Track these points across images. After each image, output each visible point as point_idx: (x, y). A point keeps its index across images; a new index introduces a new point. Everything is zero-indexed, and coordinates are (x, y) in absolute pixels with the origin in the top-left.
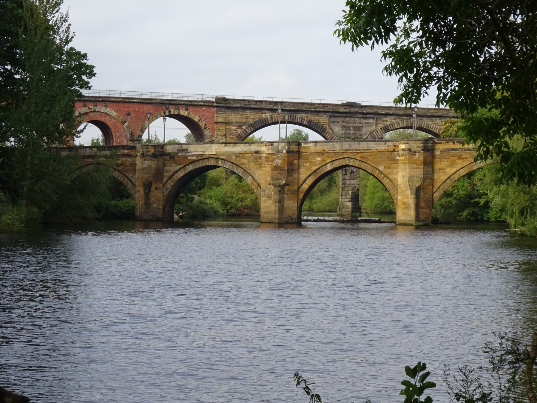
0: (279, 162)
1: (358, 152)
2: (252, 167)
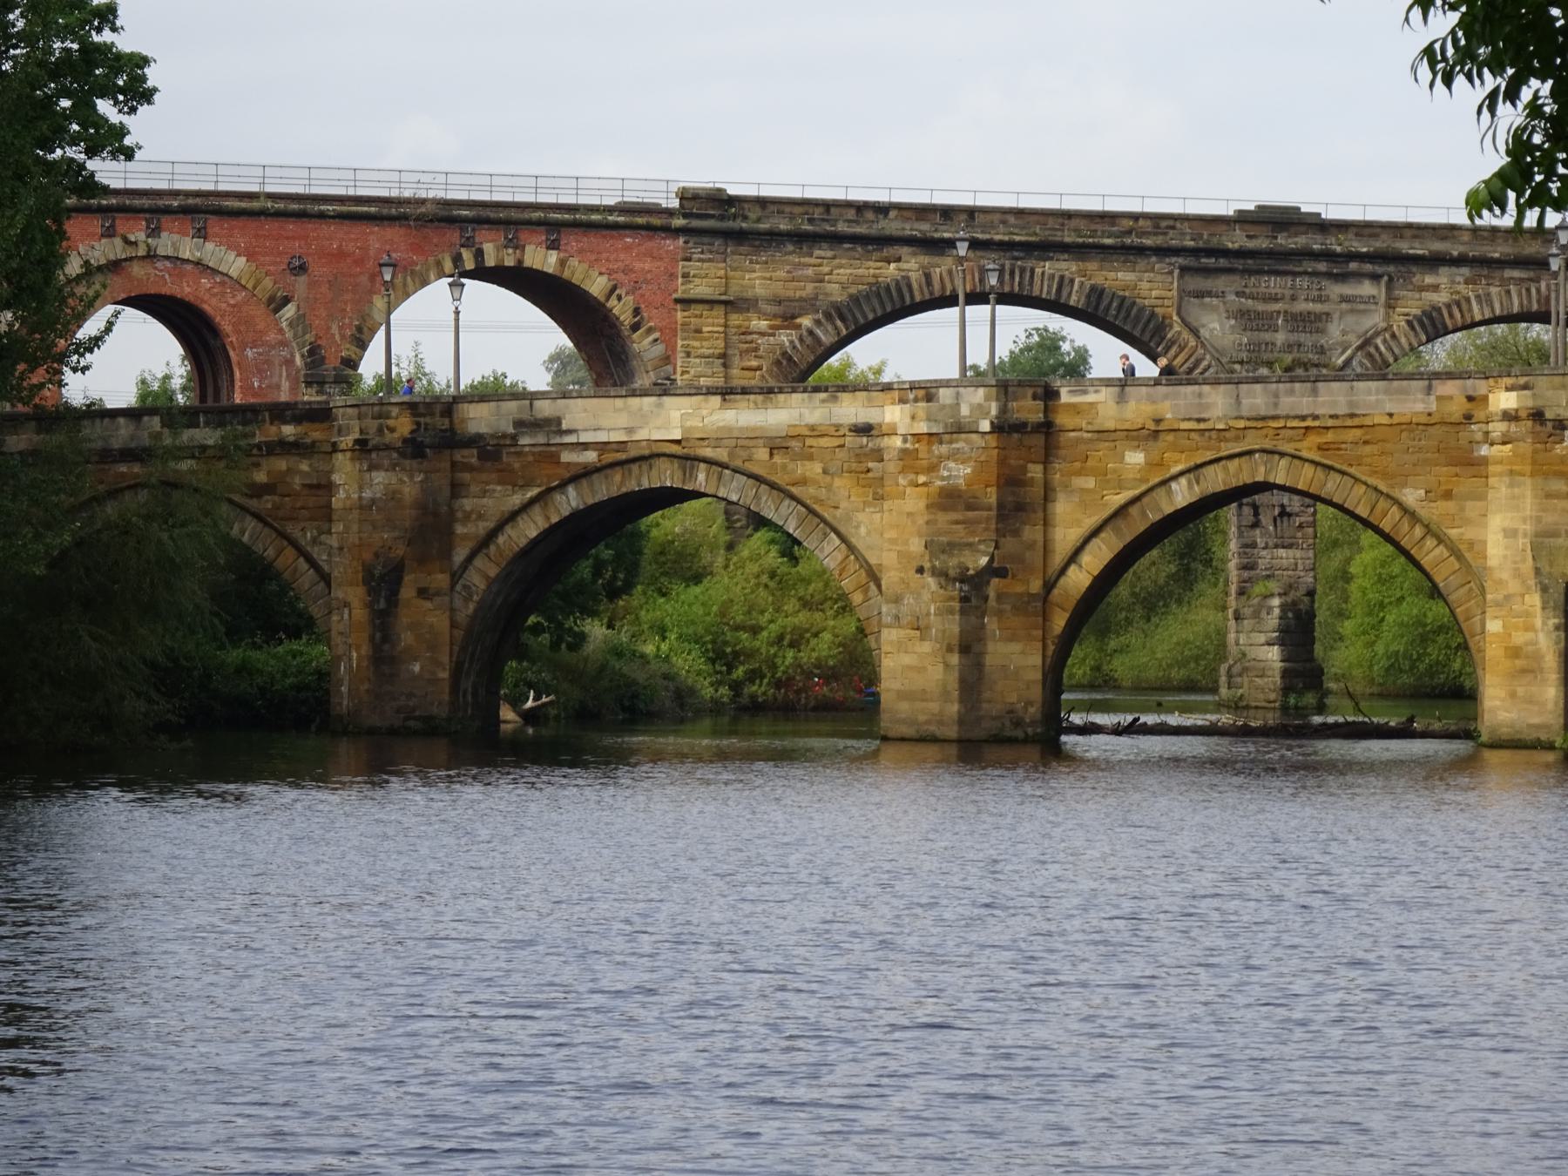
0: (959, 473)
1: (1309, 425)
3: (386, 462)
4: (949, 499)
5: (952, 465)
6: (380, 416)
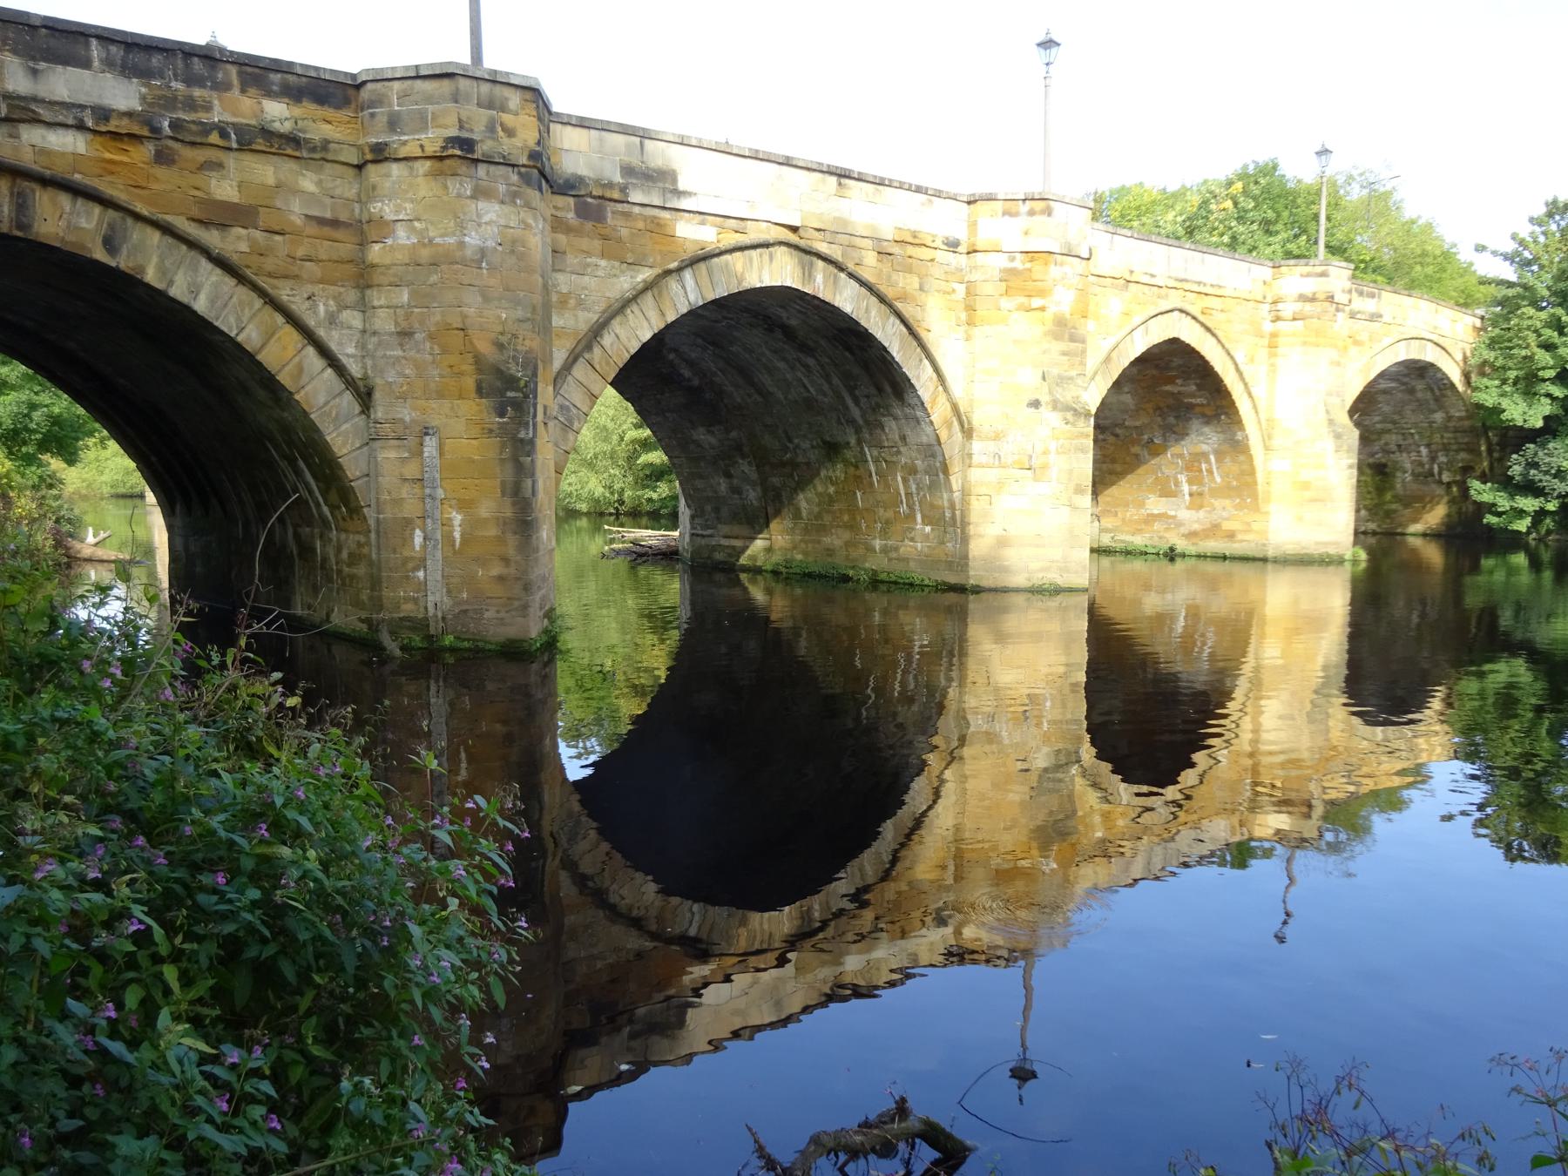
3: (502, 188)
6: (490, 106)
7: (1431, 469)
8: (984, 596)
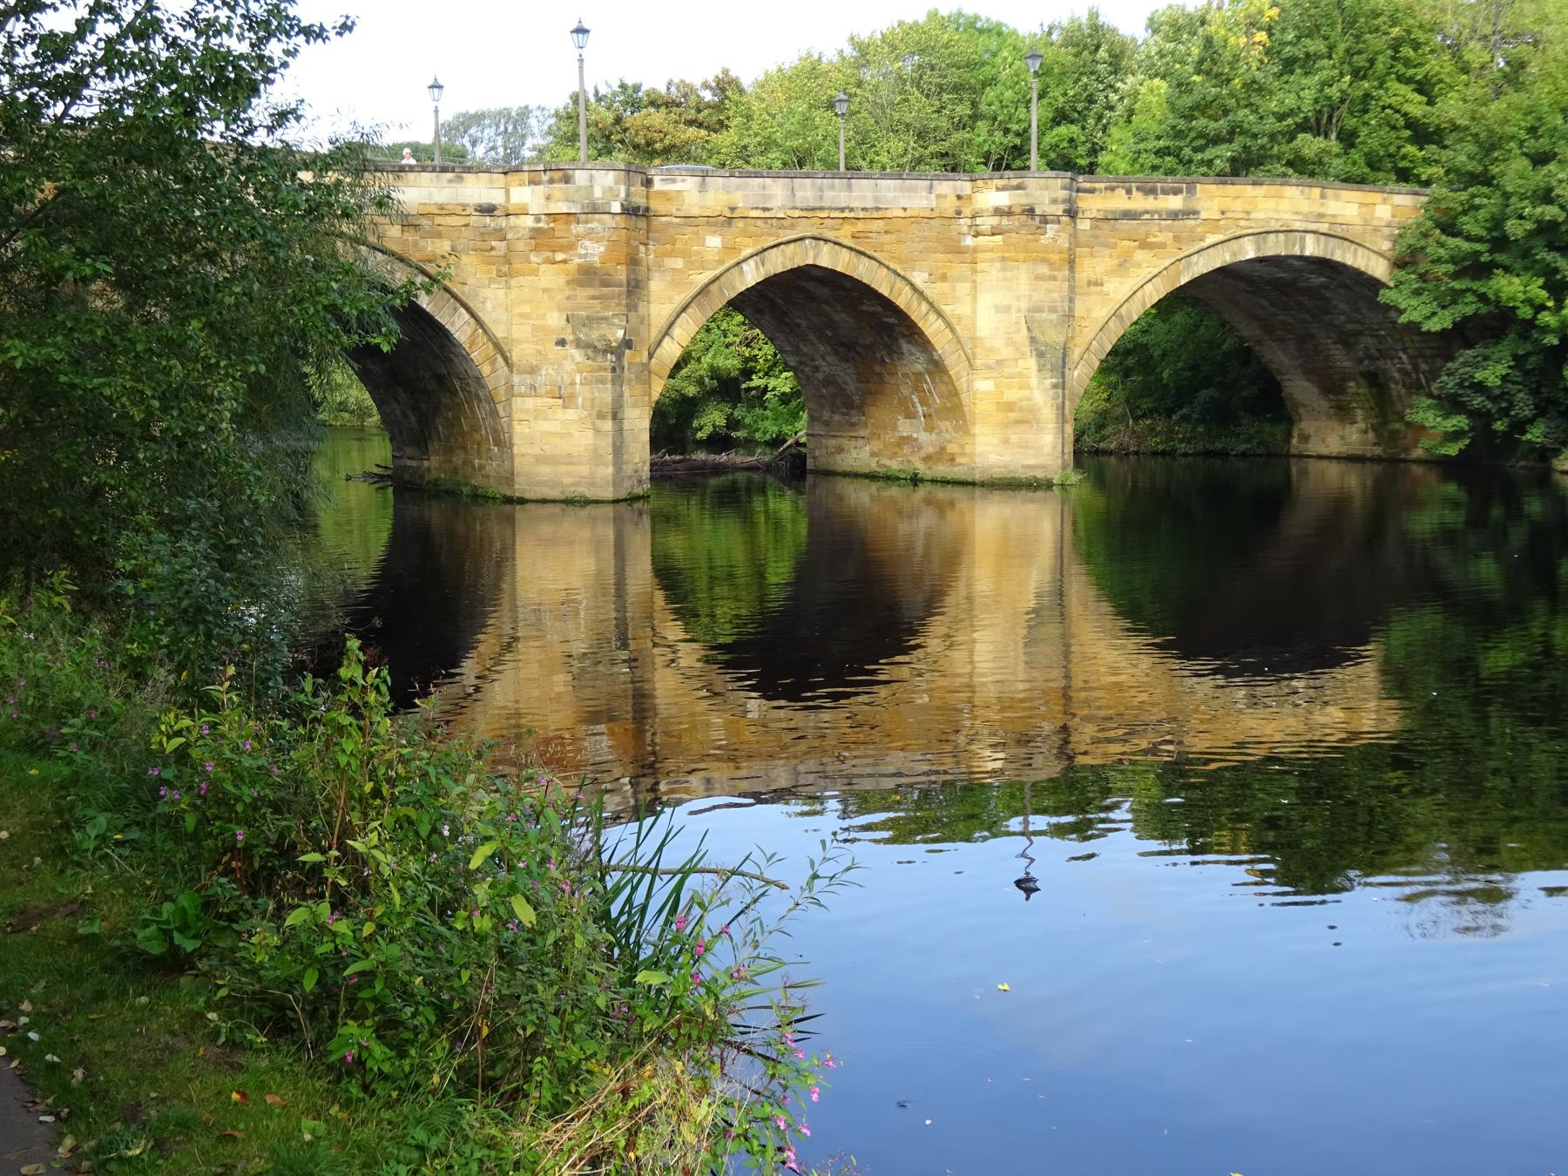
0: (594, 251)
1: (847, 215)
2: (472, 275)
4: (587, 276)
5: (588, 243)
7: (1418, 379)
8: (527, 506)
